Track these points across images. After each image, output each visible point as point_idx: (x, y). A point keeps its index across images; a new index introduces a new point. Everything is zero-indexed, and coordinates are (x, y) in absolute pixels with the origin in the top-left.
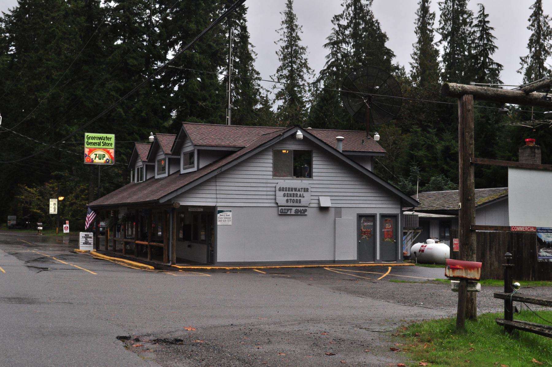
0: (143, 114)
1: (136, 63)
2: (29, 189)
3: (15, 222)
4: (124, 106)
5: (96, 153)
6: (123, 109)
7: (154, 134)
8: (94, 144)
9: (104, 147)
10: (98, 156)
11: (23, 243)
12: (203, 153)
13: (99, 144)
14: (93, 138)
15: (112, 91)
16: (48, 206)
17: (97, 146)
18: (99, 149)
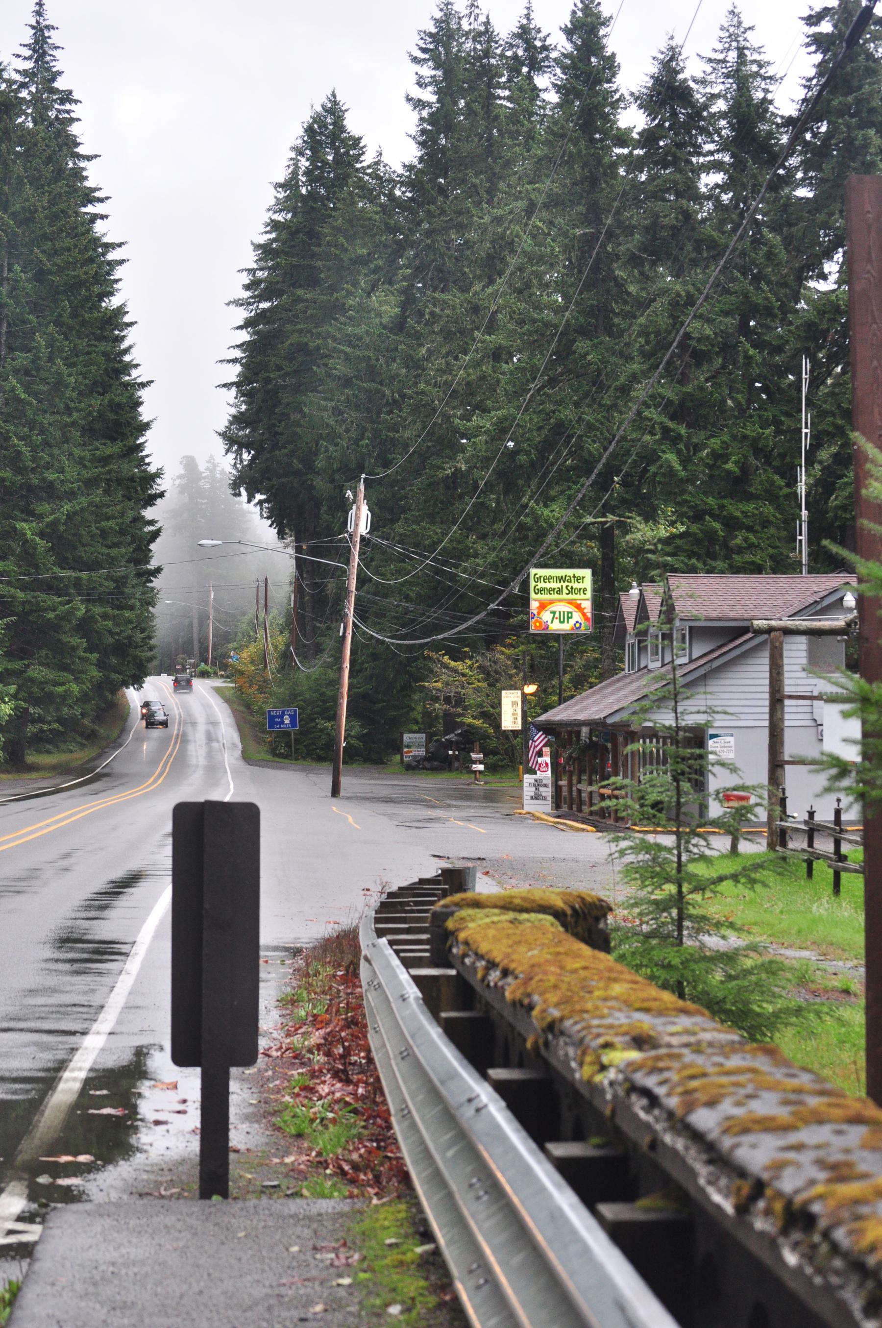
0: (730, 466)
1: (708, 331)
2: (453, 664)
3: (421, 752)
4: (681, 446)
5: (553, 609)
6: (679, 453)
7: (639, 585)
8: (550, 591)
9: (570, 596)
10: (557, 615)
11: (425, 800)
12: (698, 632)
13: (560, 591)
14: (548, 579)
15: (648, 407)
16: (499, 704)
17: (556, 596)
18: (560, 601)
